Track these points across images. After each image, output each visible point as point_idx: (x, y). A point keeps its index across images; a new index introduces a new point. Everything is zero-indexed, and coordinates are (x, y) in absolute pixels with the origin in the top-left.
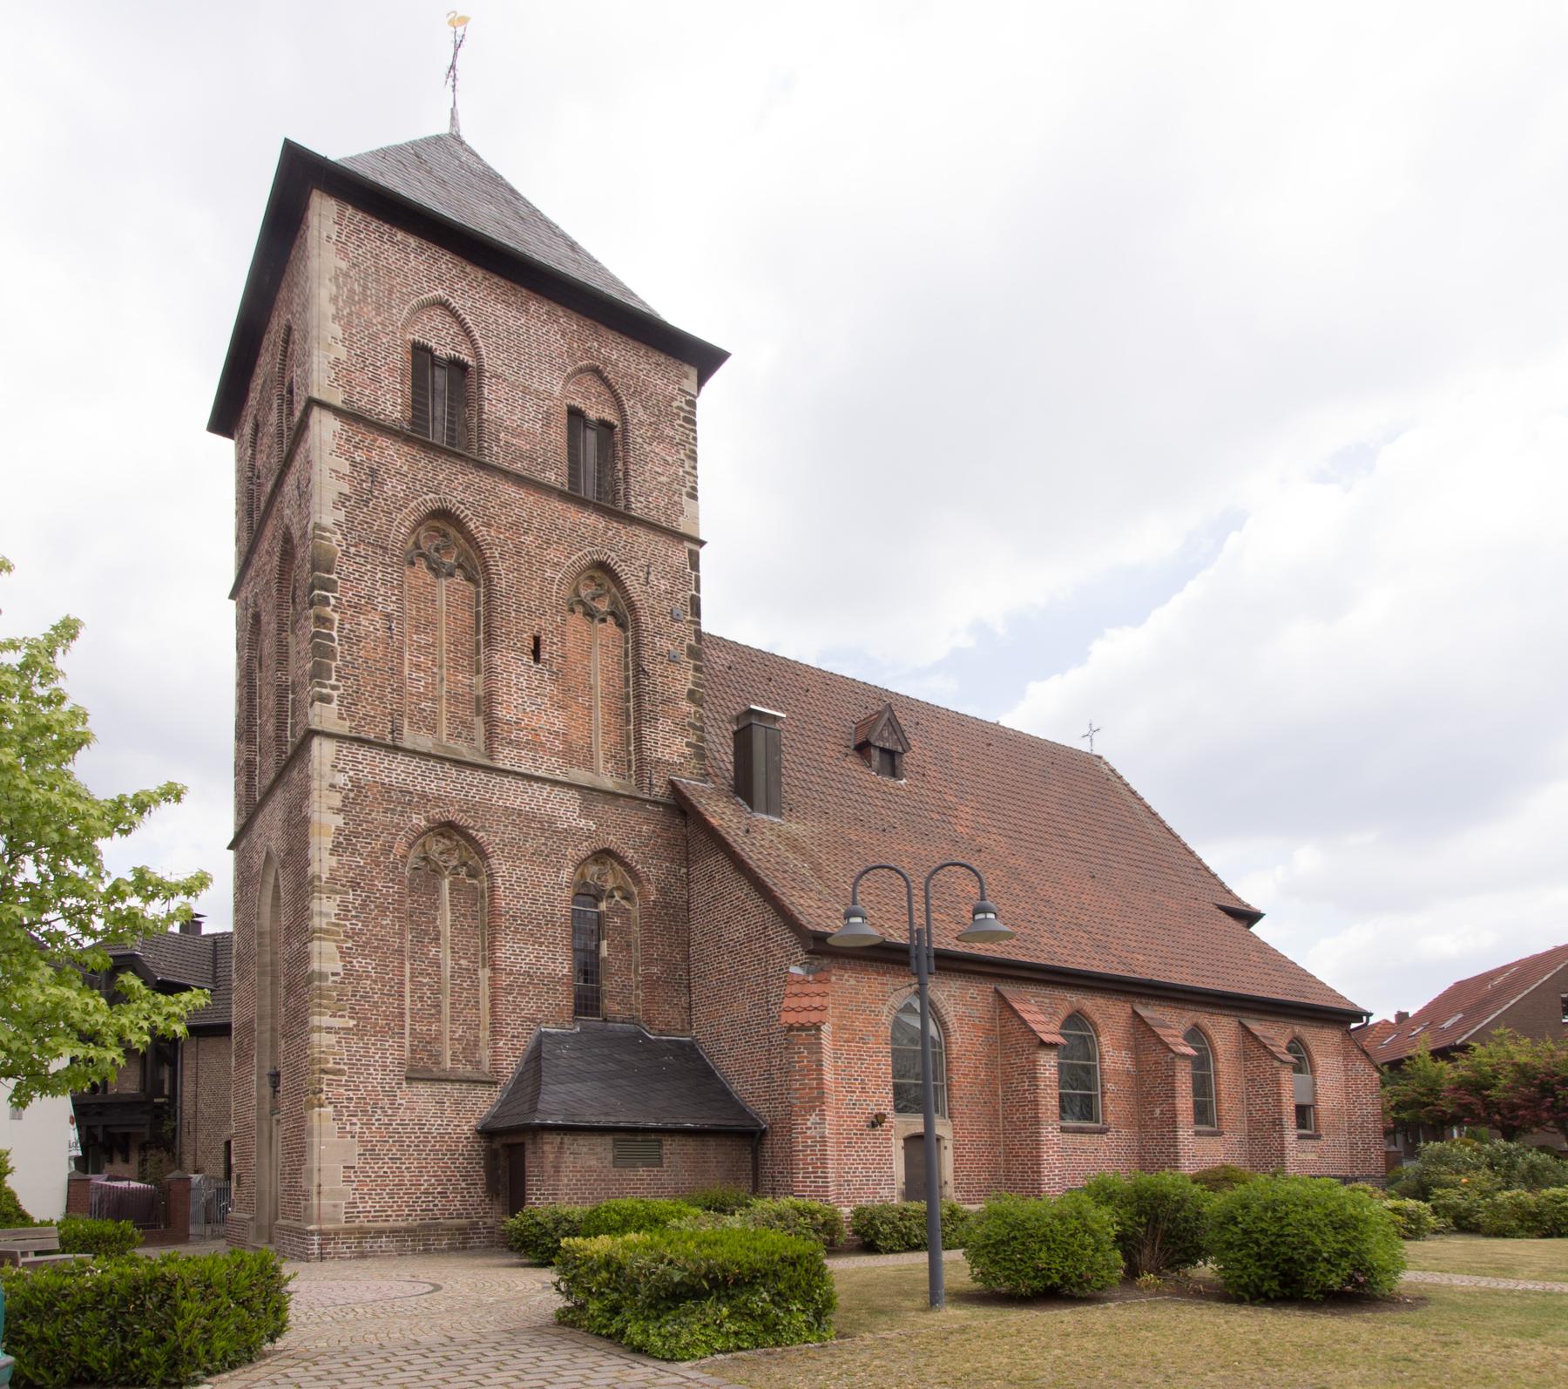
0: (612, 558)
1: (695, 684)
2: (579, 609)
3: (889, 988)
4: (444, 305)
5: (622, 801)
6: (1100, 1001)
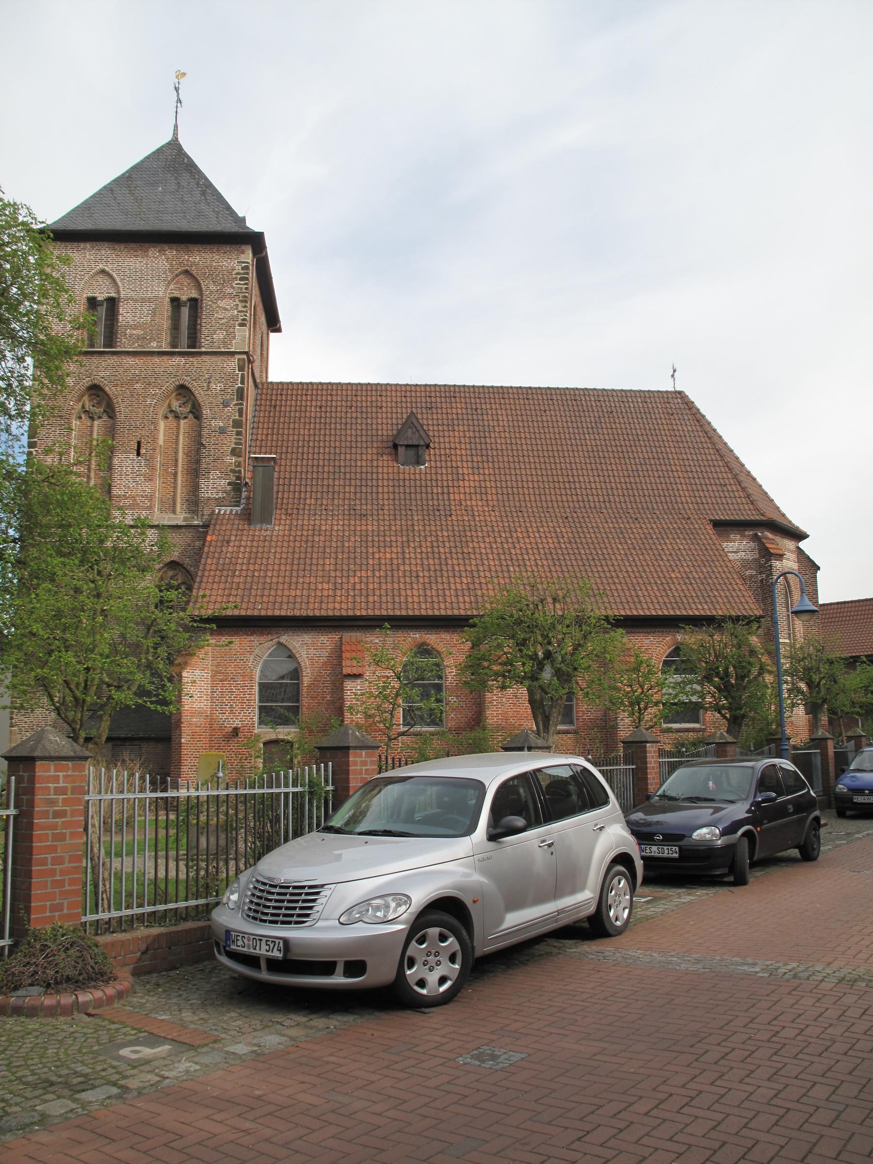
0: (187, 381)
1: (236, 444)
2: (170, 416)
3: (256, 643)
4: (103, 272)
5: (183, 530)
6: (445, 636)
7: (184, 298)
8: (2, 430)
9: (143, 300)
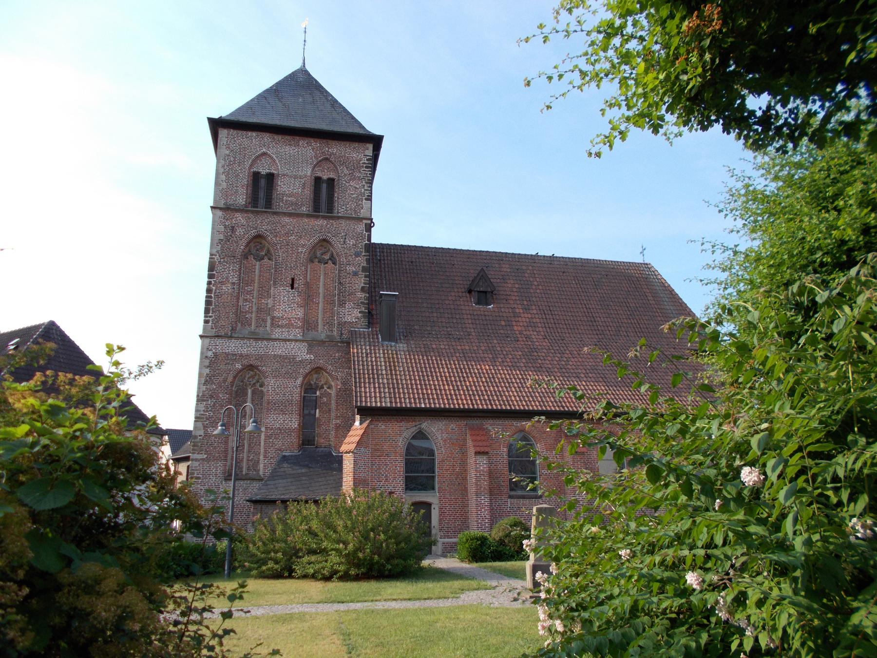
7: (325, 177)
8: (875, 227)
9: (295, 177)
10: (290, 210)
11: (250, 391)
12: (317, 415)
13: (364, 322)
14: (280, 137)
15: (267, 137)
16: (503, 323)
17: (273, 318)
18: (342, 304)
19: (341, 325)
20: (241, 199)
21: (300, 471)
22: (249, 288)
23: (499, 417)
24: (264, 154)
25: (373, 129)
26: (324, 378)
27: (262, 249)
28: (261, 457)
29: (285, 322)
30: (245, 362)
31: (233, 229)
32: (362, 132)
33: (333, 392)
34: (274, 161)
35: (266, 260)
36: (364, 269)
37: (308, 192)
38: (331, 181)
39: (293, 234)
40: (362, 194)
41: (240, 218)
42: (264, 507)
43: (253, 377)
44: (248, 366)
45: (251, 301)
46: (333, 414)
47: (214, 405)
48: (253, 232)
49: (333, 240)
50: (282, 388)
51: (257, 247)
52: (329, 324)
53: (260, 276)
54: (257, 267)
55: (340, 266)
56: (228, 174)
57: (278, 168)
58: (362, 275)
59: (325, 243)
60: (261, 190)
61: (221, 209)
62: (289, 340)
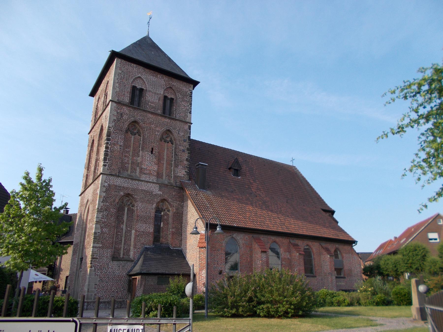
7: (169, 97)
9: (155, 93)
10: (152, 110)
11: (126, 209)
12: (162, 226)
13: (187, 177)
14: (148, 70)
15: (141, 69)
16: (247, 187)
17: (141, 169)
18: (176, 166)
19: (176, 177)
20: (127, 100)
21: (158, 257)
22: (127, 150)
23: (266, 234)
24: (139, 77)
25: (193, 76)
26: (166, 206)
27: (135, 129)
28: (132, 248)
29: (148, 172)
30: (126, 192)
31: (121, 115)
32: (186, 76)
33: (170, 214)
34: (145, 82)
35: (137, 135)
36: (188, 149)
37: (161, 103)
38: (172, 99)
39: (155, 125)
40: (188, 110)
41: (125, 110)
42: (147, 277)
43: (128, 201)
44: (127, 194)
45: (128, 157)
46: (170, 226)
47: (107, 215)
48: (132, 119)
49: (173, 131)
50: (144, 208)
51: (133, 128)
52: (169, 176)
53: (134, 144)
54: (133, 139)
55: (176, 145)
56: (120, 84)
57: (147, 87)
58: (187, 152)
59: (168, 132)
60: (137, 95)
61: (115, 102)
62: (149, 182)
